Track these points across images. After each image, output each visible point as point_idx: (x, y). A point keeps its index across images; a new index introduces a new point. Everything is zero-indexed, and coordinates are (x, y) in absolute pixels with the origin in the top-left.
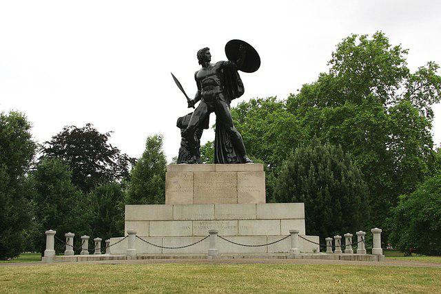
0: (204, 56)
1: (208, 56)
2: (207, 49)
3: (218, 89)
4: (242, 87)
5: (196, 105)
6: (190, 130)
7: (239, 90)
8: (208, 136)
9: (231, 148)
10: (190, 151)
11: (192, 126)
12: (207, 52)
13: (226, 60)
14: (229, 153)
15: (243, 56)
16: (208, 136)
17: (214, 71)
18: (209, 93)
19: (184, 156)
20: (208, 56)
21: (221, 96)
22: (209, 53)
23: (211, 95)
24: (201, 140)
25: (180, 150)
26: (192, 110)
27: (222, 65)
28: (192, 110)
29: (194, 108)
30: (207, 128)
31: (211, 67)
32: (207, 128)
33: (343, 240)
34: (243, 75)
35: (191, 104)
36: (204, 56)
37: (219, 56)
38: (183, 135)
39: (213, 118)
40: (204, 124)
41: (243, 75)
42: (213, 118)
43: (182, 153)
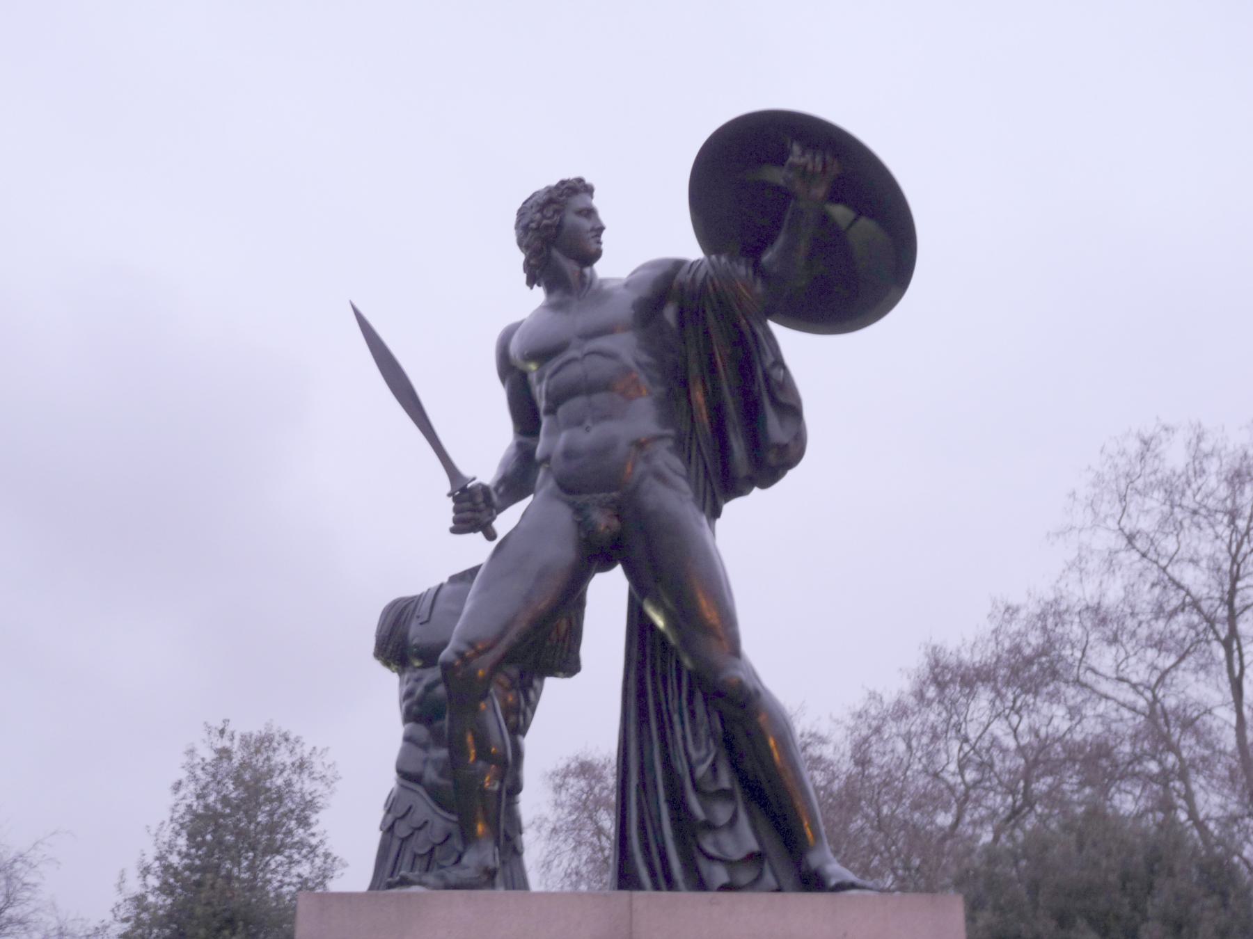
0: (557, 234)
1: (587, 224)
2: (454, 531)
3: (641, 418)
4: (792, 411)
5: (507, 521)
6: (462, 686)
7: (775, 429)
8: (577, 720)
9: (726, 795)
10: (457, 799)
11: (475, 648)
12: (578, 202)
13: (690, 249)
14: (709, 826)
15: (805, 218)
16: (577, 720)
17: (622, 309)
18: (586, 438)
19: (420, 845)
20: (587, 224)
21: (666, 458)
22: (590, 212)
23: (603, 450)
24: (530, 742)
25: (390, 807)
26: (475, 550)
27: (666, 289)
28: (475, 550)
29: (490, 536)
30: (568, 665)
31: (600, 294)
32: (568, 665)
33: (1133, 709)
34: (801, 351)
35: (473, 508)
36: (557, 234)
37: (649, 231)
38: (420, 711)
39: (608, 593)
40: (547, 644)
41: (801, 351)
42: (608, 593)
43: (402, 830)
